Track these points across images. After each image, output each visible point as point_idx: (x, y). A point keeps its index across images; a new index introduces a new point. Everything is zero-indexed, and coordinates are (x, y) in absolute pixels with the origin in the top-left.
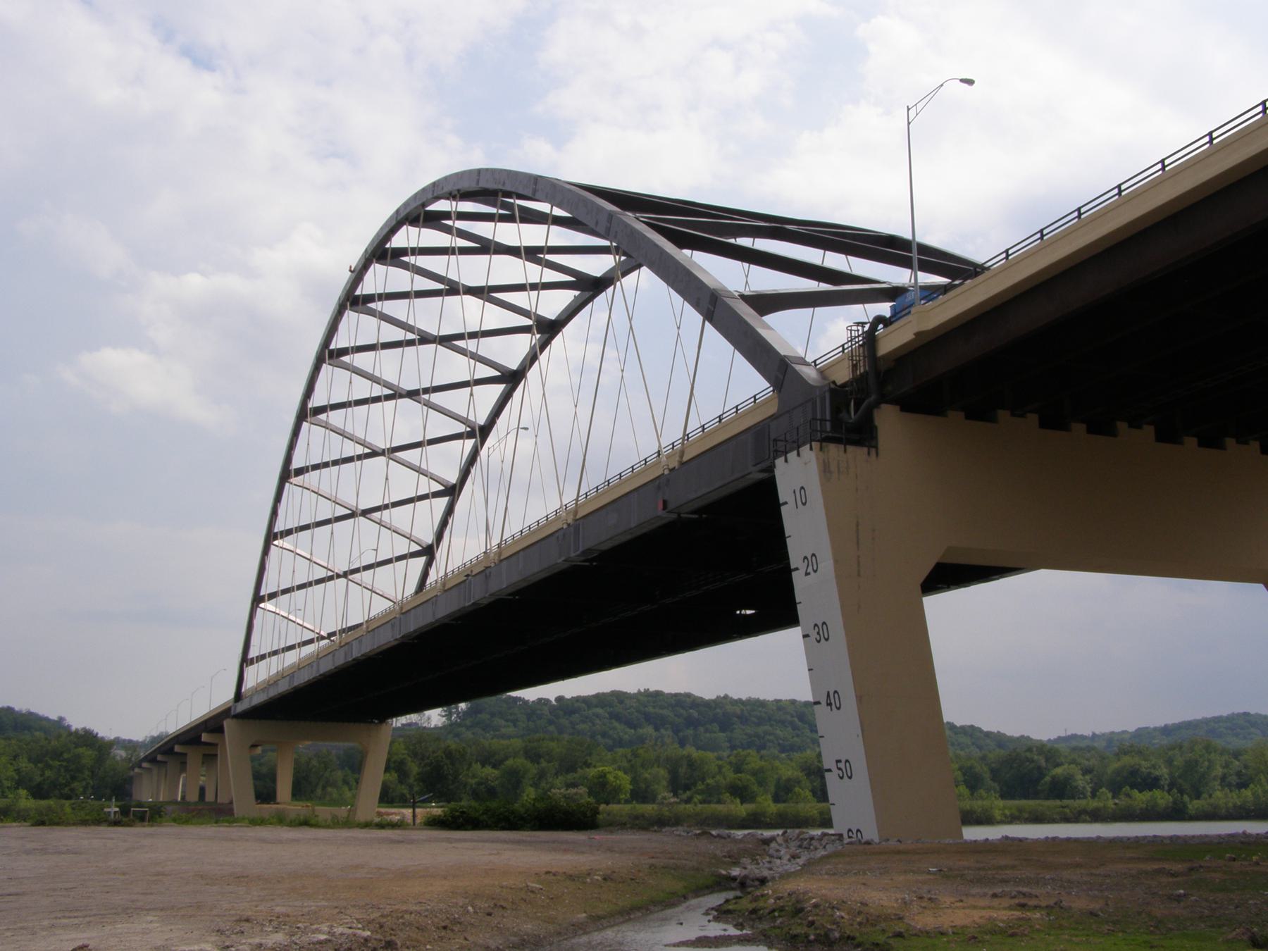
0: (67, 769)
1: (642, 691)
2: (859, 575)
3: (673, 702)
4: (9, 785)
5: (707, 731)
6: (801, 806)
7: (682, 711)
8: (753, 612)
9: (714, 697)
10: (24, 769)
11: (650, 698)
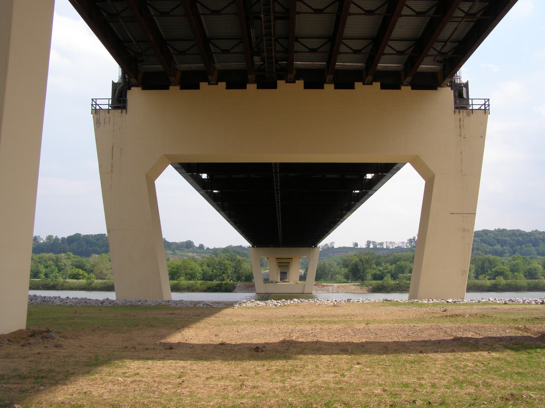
0: (221, 269)
1: (497, 229)
2: (112, 172)
3: (511, 234)
4: (200, 275)
5: (526, 246)
6: (518, 281)
7: (515, 238)
8: (217, 192)
9: (530, 231)
10: (205, 269)
11: (500, 233)
